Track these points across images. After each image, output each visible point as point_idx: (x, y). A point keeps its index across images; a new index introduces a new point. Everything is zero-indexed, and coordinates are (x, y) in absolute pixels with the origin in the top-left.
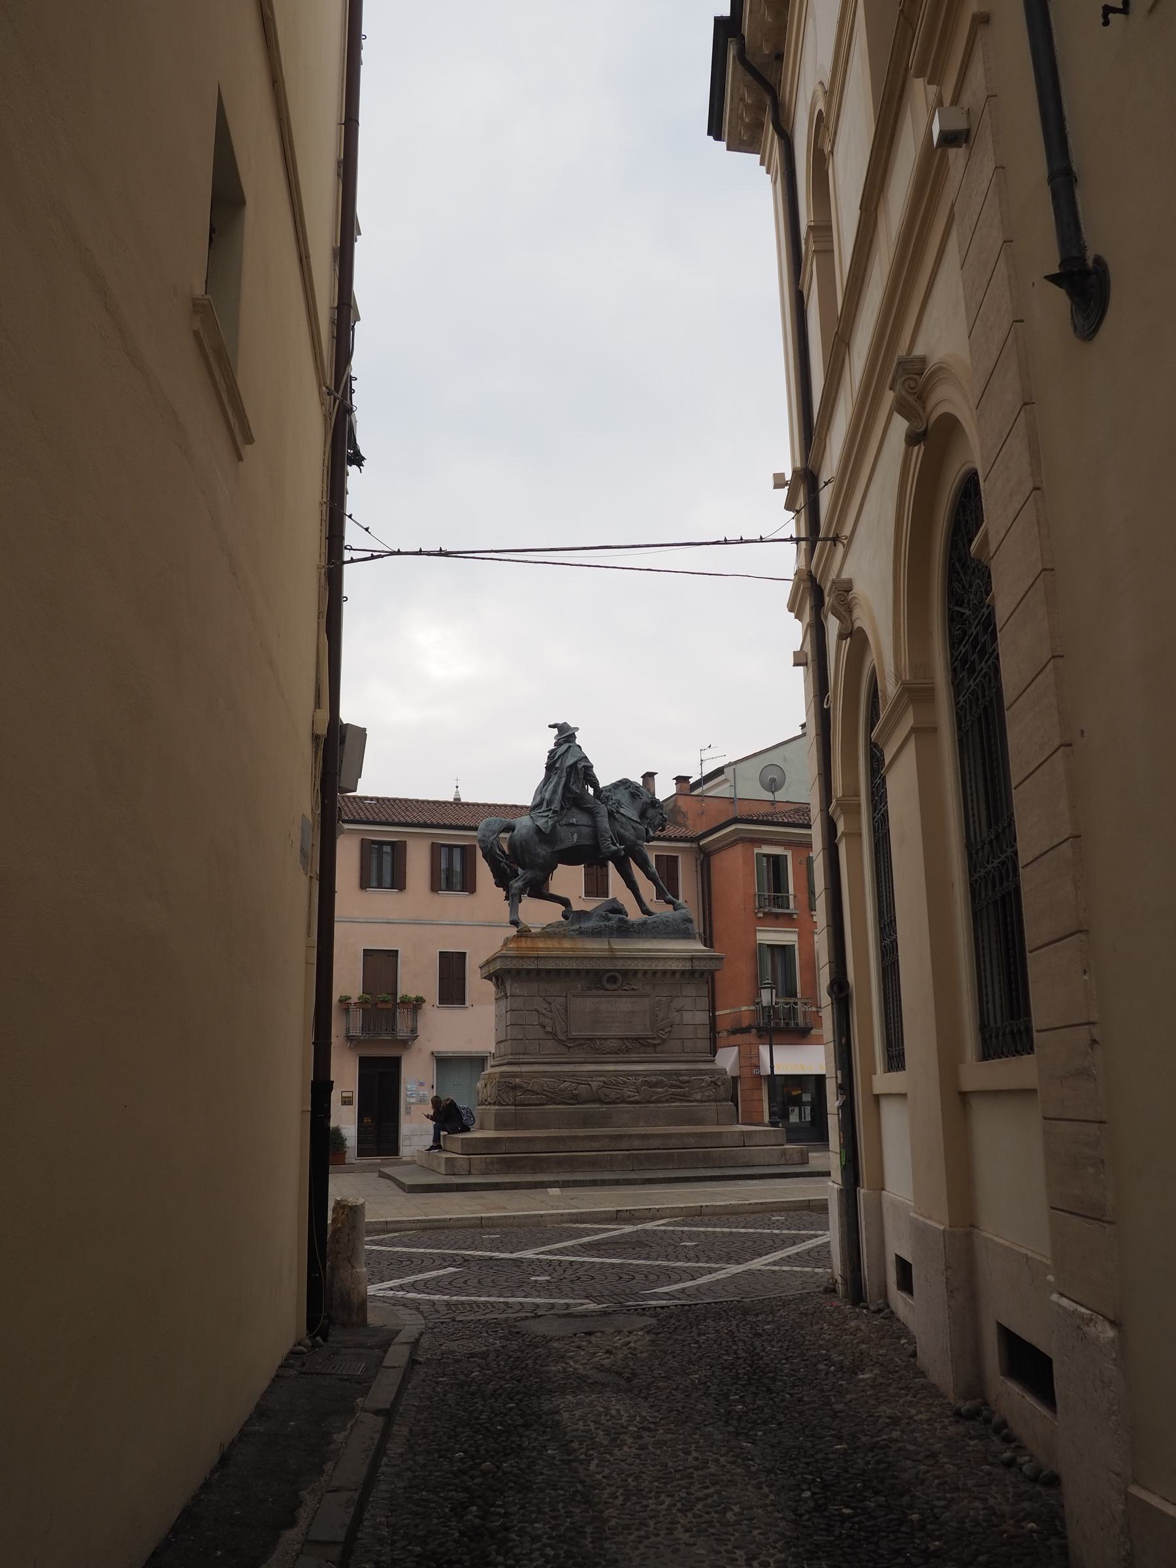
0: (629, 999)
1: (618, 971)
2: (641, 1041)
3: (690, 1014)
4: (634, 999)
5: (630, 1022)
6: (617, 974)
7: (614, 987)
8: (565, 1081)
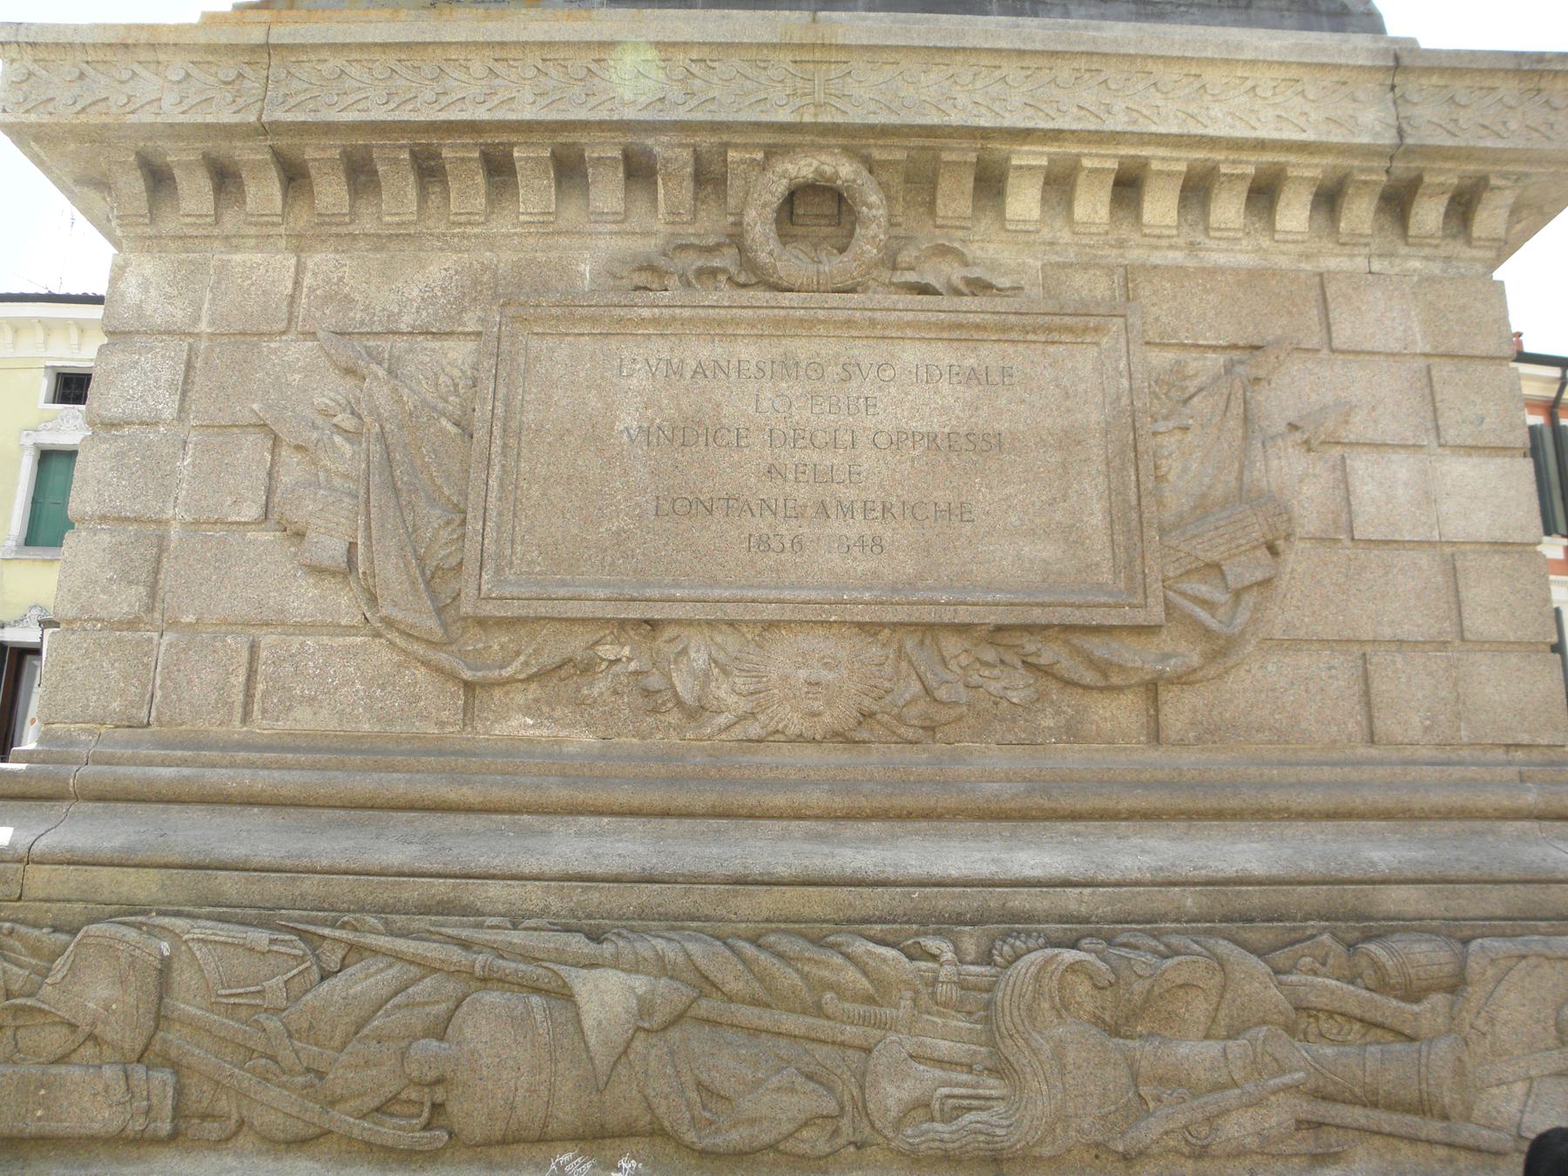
0: (944, 355)
1: (853, 139)
2: (1050, 653)
3: (1402, 468)
4: (989, 355)
5: (959, 512)
6: (846, 170)
7: (834, 265)
8: (356, 951)
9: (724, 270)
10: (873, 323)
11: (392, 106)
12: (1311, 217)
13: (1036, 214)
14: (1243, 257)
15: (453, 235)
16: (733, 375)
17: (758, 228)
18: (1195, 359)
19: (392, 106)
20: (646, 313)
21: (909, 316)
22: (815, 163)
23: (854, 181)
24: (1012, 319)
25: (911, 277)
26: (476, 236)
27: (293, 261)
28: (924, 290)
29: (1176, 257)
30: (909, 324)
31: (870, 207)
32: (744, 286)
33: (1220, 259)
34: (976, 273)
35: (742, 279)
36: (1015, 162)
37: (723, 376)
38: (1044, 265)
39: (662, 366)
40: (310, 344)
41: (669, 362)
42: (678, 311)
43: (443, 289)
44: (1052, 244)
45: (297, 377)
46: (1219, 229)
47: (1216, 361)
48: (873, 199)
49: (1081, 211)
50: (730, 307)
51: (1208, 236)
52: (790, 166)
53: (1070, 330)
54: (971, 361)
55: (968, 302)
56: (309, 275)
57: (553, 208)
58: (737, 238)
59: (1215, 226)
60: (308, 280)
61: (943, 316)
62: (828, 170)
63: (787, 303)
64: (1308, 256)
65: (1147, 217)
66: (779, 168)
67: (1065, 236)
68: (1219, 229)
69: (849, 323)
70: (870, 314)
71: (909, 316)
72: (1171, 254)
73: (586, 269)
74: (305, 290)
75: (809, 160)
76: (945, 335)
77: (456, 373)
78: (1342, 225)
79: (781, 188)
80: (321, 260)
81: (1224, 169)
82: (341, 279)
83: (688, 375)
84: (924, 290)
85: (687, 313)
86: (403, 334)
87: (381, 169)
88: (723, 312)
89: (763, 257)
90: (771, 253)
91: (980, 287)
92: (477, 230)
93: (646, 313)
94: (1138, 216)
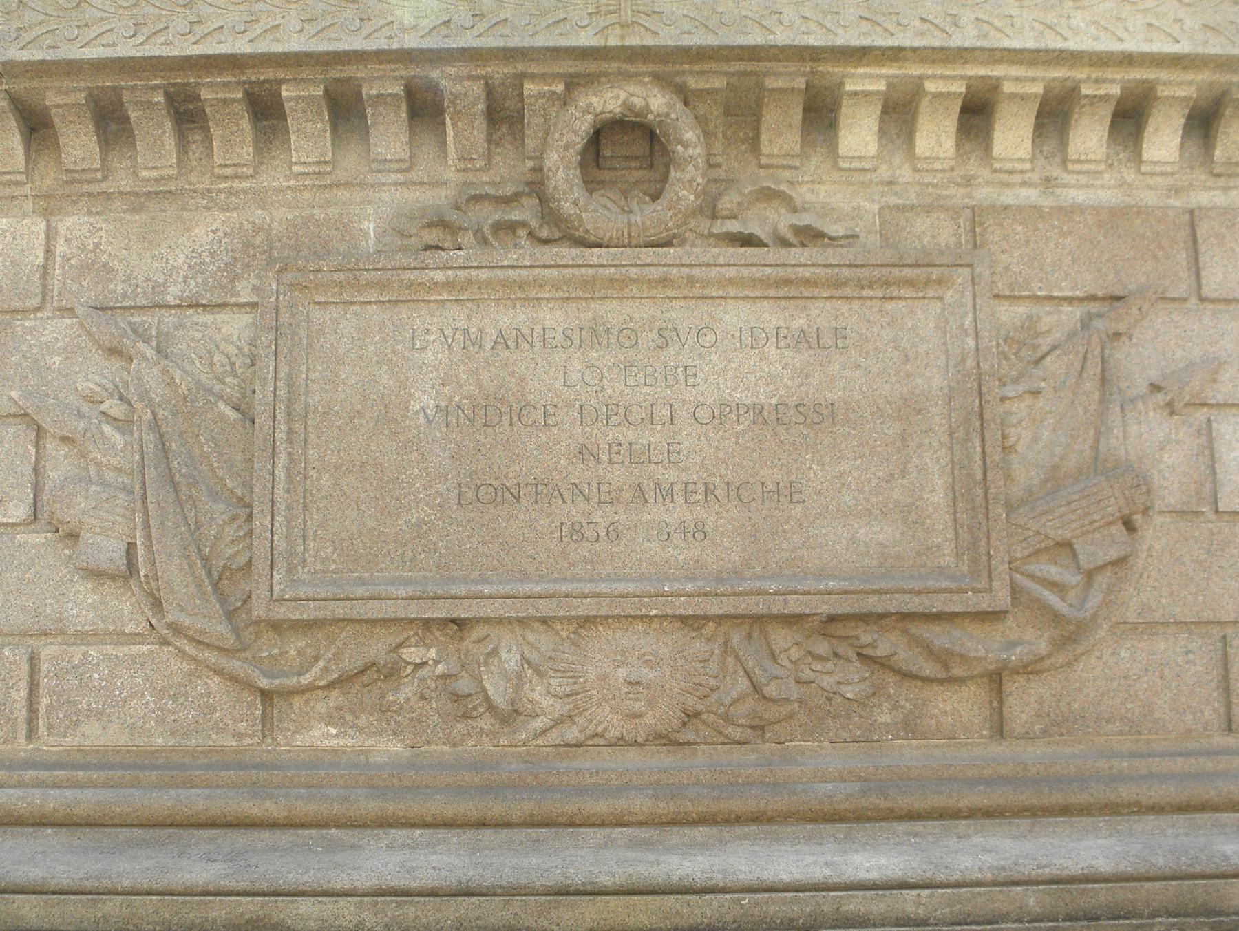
6: (658, 102)
9: (523, 224)
10: (691, 281)
11: (141, 39)
12: (1182, 145)
13: (873, 149)
14: (1106, 196)
15: (219, 191)
16: (538, 345)
17: (561, 173)
18: (1049, 313)
19: (141, 39)
20: (439, 276)
21: (731, 272)
22: (623, 95)
23: (667, 115)
24: (846, 272)
25: (733, 226)
26: (245, 192)
27: (43, 226)
28: (747, 241)
29: (1030, 195)
30: (731, 281)
31: (686, 145)
32: (547, 242)
33: (1079, 196)
34: (806, 219)
35: (544, 234)
36: (849, 87)
37: (526, 346)
38: (881, 209)
39: (459, 336)
40: (68, 321)
41: (466, 332)
42: (474, 273)
43: (212, 255)
44: (890, 183)
45: (57, 359)
46: (1078, 161)
47: (1072, 314)
48: (689, 135)
49: (923, 144)
50: (531, 266)
51: (1065, 169)
52: (594, 100)
53: (910, 283)
54: (801, 322)
55: (797, 254)
56: (62, 241)
57: (329, 157)
58: (537, 186)
59: (1075, 157)
60: (60, 248)
61: (768, 270)
62: (638, 102)
63: (595, 261)
64: (1177, 191)
65: (997, 150)
66: (582, 102)
67: (906, 174)
68: (1078, 161)
69: (664, 282)
70: (687, 270)
71: (731, 272)
72: (1024, 192)
73: (369, 226)
74: (58, 259)
75: (616, 91)
76: (772, 293)
77: (232, 350)
78: (1217, 152)
79: (585, 126)
80: (73, 224)
81: (1086, 90)
82: (97, 245)
83: (488, 346)
84: (747, 241)
85: (484, 275)
86: (170, 307)
87: (133, 115)
88: (524, 272)
89: (567, 207)
90: (575, 203)
91: (810, 236)
92: (246, 184)
93: (439, 276)
94: (988, 149)
